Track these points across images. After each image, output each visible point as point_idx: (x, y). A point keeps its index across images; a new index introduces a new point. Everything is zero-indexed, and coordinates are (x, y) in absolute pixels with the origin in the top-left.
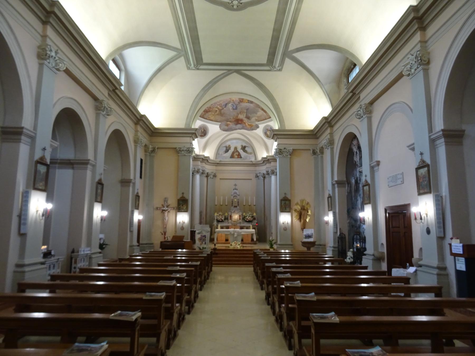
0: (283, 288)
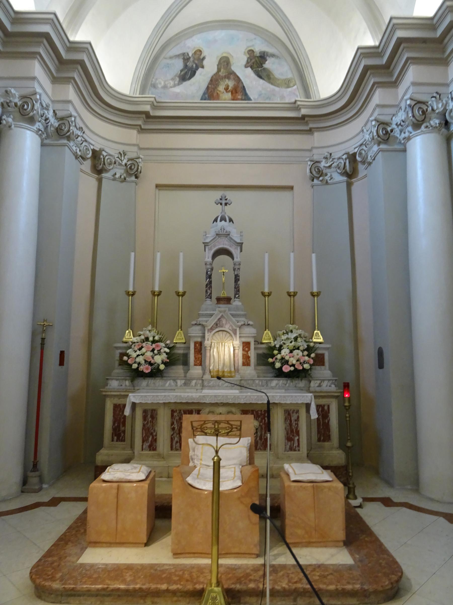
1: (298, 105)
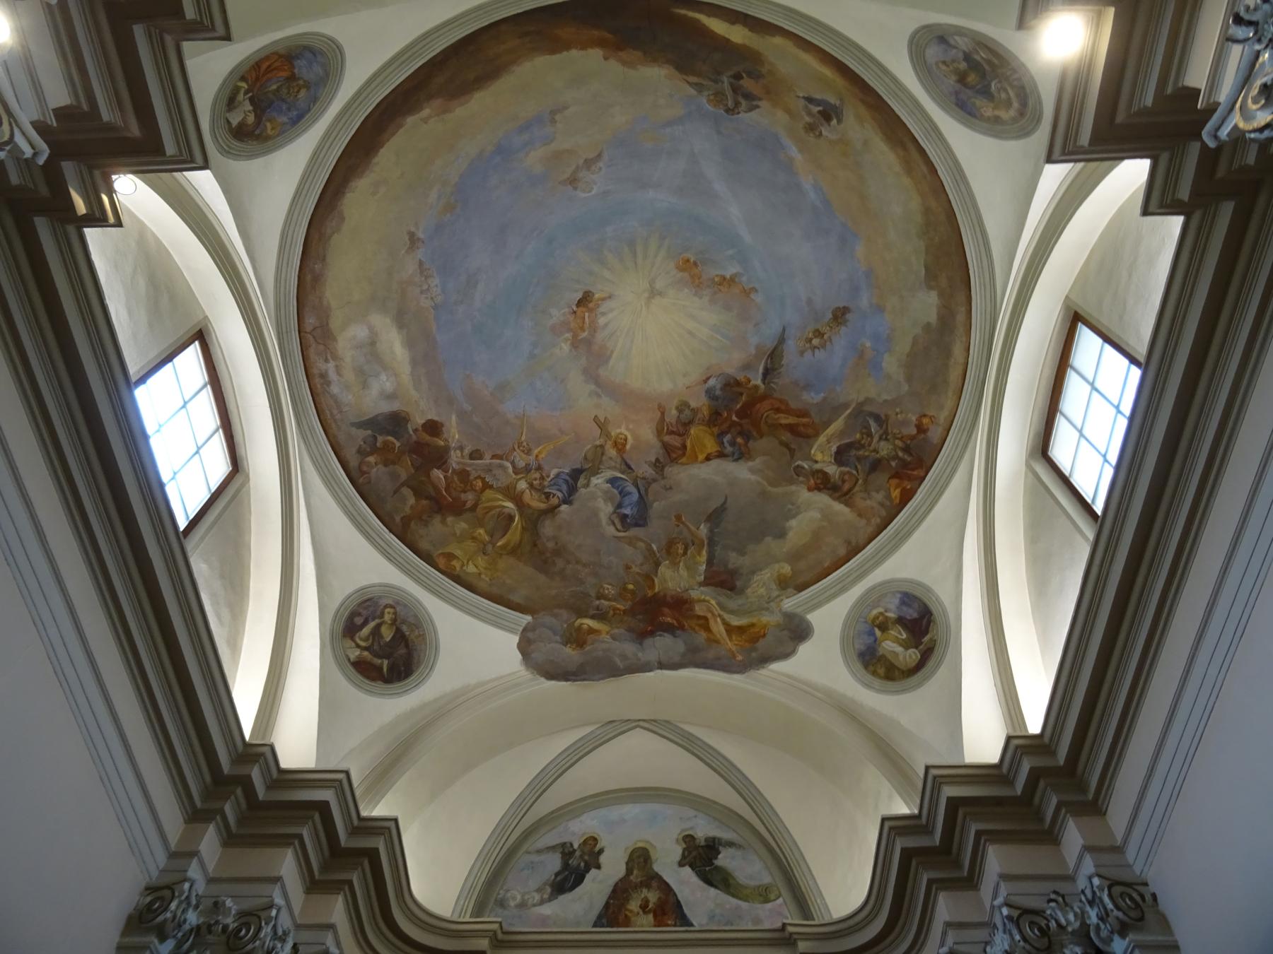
0: (71, 206)
1: (791, 934)
